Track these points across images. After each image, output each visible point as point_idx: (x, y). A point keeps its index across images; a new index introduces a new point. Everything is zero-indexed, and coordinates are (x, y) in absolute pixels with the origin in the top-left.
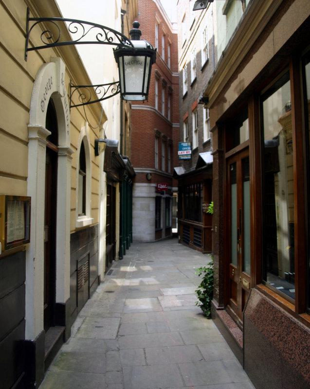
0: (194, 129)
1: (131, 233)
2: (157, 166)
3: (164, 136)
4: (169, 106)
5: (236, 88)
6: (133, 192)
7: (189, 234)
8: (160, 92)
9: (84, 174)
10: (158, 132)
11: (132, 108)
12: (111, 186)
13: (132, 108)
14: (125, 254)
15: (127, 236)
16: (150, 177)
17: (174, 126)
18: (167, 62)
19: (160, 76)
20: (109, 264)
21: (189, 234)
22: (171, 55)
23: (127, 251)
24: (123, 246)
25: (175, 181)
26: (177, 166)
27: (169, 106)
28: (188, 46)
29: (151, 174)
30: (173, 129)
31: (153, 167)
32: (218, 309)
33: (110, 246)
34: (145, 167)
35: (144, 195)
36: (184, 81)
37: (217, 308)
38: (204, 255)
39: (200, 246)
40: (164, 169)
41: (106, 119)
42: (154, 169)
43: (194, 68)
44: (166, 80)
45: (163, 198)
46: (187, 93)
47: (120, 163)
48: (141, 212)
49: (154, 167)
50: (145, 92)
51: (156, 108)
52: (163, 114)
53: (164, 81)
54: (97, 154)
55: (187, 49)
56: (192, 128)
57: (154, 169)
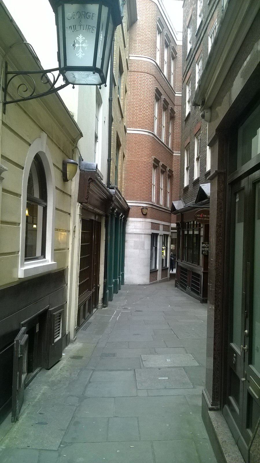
0: (196, 157)
1: (123, 275)
2: (154, 199)
3: (163, 166)
4: (170, 131)
5: (201, 276)
6: (127, 227)
7: (186, 278)
9: (45, 204)
10: (156, 161)
12: (93, 220)
13: (128, 132)
14: (111, 300)
15: (115, 277)
16: (145, 211)
17: (174, 154)
18: (170, 78)
19: (160, 94)
20: (82, 320)
21: (186, 278)
22: (175, 70)
23: (115, 296)
24: (108, 291)
25: (174, 217)
27: (170, 131)
30: (174, 158)
32: (211, 409)
33: (88, 294)
35: (138, 231)
37: (210, 406)
38: (201, 304)
39: (198, 293)
40: (162, 202)
41: (81, 135)
44: (168, 100)
45: (160, 235)
46: (189, 114)
47: (106, 194)
48: (135, 250)
50: (98, 66)
51: (156, 133)
52: (163, 140)
53: (165, 101)
54: (65, 179)
56: (194, 155)
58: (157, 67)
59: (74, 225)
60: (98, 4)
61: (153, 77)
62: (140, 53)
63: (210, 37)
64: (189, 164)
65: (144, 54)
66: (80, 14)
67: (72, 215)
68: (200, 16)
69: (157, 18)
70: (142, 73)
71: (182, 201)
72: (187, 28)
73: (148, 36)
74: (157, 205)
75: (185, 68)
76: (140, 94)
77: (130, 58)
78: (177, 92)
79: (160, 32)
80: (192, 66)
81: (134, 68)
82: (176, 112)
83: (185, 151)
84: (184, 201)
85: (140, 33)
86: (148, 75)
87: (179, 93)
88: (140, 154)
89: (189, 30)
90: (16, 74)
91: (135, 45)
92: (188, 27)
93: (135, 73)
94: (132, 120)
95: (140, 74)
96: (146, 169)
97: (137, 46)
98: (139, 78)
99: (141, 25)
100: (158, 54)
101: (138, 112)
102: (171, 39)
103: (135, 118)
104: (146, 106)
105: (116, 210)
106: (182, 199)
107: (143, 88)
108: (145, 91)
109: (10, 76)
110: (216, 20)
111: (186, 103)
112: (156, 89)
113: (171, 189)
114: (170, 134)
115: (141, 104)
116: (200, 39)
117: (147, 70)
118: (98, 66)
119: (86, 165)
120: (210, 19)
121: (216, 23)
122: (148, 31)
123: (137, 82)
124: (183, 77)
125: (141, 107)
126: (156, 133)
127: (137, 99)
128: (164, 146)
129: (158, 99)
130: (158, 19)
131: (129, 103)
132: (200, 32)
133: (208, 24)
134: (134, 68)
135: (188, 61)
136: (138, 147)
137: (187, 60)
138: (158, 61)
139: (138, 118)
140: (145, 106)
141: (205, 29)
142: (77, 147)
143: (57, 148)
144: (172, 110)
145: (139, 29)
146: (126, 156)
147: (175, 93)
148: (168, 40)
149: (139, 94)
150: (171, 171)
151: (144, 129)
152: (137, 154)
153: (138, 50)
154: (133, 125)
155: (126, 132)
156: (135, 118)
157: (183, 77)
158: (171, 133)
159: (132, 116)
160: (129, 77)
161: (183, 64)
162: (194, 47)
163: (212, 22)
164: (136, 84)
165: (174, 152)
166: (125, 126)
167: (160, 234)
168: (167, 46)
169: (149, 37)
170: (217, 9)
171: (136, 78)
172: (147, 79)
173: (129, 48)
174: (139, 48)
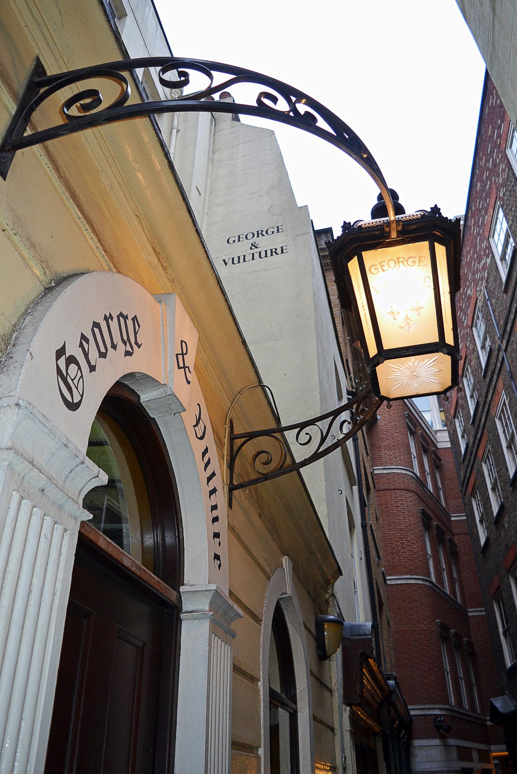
3: (456, 635)
4: (455, 576)
6: (412, 760)
8: (433, 548)
10: (444, 627)
11: (389, 582)
13: (389, 582)
18: (438, 495)
19: (430, 519)
26: (496, 695)
27: (455, 576)
28: (474, 453)
29: (441, 715)
31: (447, 701)
34: (429, 703)
36: (478, 519)
42: (447, 706)
43: (481, 521)
44: (443, 527)
49: (448, 702)
50: (449, 340)
53: (438, 527)
55: (472, 460)
57: (447, 706)
58: (418, 480)
59: (344, 755)
60: (427, 241)
61: (414, 494)
62: (389, 463)
63: (499, 419)
64: (507, 624)
65: (395, 464)
66: (395, 262)
67: (338, 732)
68: (472, 397)
69: (405, 414)
70: (397, 491)
71: (508, 696)
72: (453, 419)
73: (396, 438)
74: (459, 710)
75: (462, 474)
76: (399, 522)
77: (376, 472)
78: (452, 514)
79: (412, 433)
80: (475, 468)
81: (383, 485)
82: (458, 544)
83: (493, 602)
84: (512, 697)
85: (384, 436)
86: (407, 492)
87: (456, 515)
88: (414, 618)
89: (456, 420)
90: (247, 438)
91: (379, 453)
92: (454, 417)
93: (386, 492)
94: (392, 562)
95: (394, 493)
96: (430, 643)
97: (383, 454)
98: (393, 498)
99: (383, 426)
100: (415, 463)
101: (400, 549)
102: (429, 440)
103: (397, 558)
104: (412, 538)
105: (397, 722)
106: (506, 692)
107: (402, 512)
108: (406, 516)
109: (238, 442)
110: (503, 392)
111: (476, 525)
112: (422, 511)
113: (459, 573)
114: (456, 581)
115: (403, 537)
116: (481, 426)
117: (403, 485)
118: (449, 340)
119: (353, 627)
120: (491, 394)
121: (505, 396)
122: (395, 432)
123: (391, 504)
124: (462, 487)
125: (404, 541)
126: (433, 579)
127: (396, 529)
128: (450, 601)
129: (427, 526)
130: (407, 415)
131: (384, 536)
132: (479, 416)
133: (490, 401)
134: (383, 485)
135: (466, 463)
136: (410, 605)
137: (463, 462)
138: (417, 471)
139: (401, 558)
140: (409, 539)
141: (486, 410)
142: (333, 595)
143: (306, 594)
144: (451, 541)
145: (382, 431)
146: (392, 623)
147: (451, 517)
148: (425, 443)
149: (397, 522)
150: (470, 644)
151: (414, 575)
152: (410, 619)
153: (385, 459)
154: (395, 570)
155: (385, 582)
156: (397, 558)
157: (462, 487)
158: (457, 579)
159: (391, 556)
160: (378, 499)
161: (457, 469)
162: (472, 440)
163: (496, 398)
164: (390, 508)
165: (469, 610)
166: (383, 572)
167: (475, 769)
168: (426, 451)
169: (399, 441)
170: (501, 378)
171: (389, 498)
172: (406, 498)
173: (373, 458)
174: (387, 456)
